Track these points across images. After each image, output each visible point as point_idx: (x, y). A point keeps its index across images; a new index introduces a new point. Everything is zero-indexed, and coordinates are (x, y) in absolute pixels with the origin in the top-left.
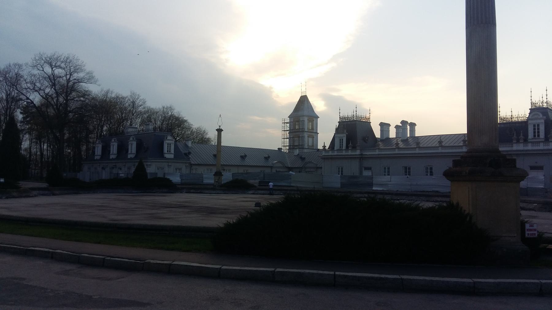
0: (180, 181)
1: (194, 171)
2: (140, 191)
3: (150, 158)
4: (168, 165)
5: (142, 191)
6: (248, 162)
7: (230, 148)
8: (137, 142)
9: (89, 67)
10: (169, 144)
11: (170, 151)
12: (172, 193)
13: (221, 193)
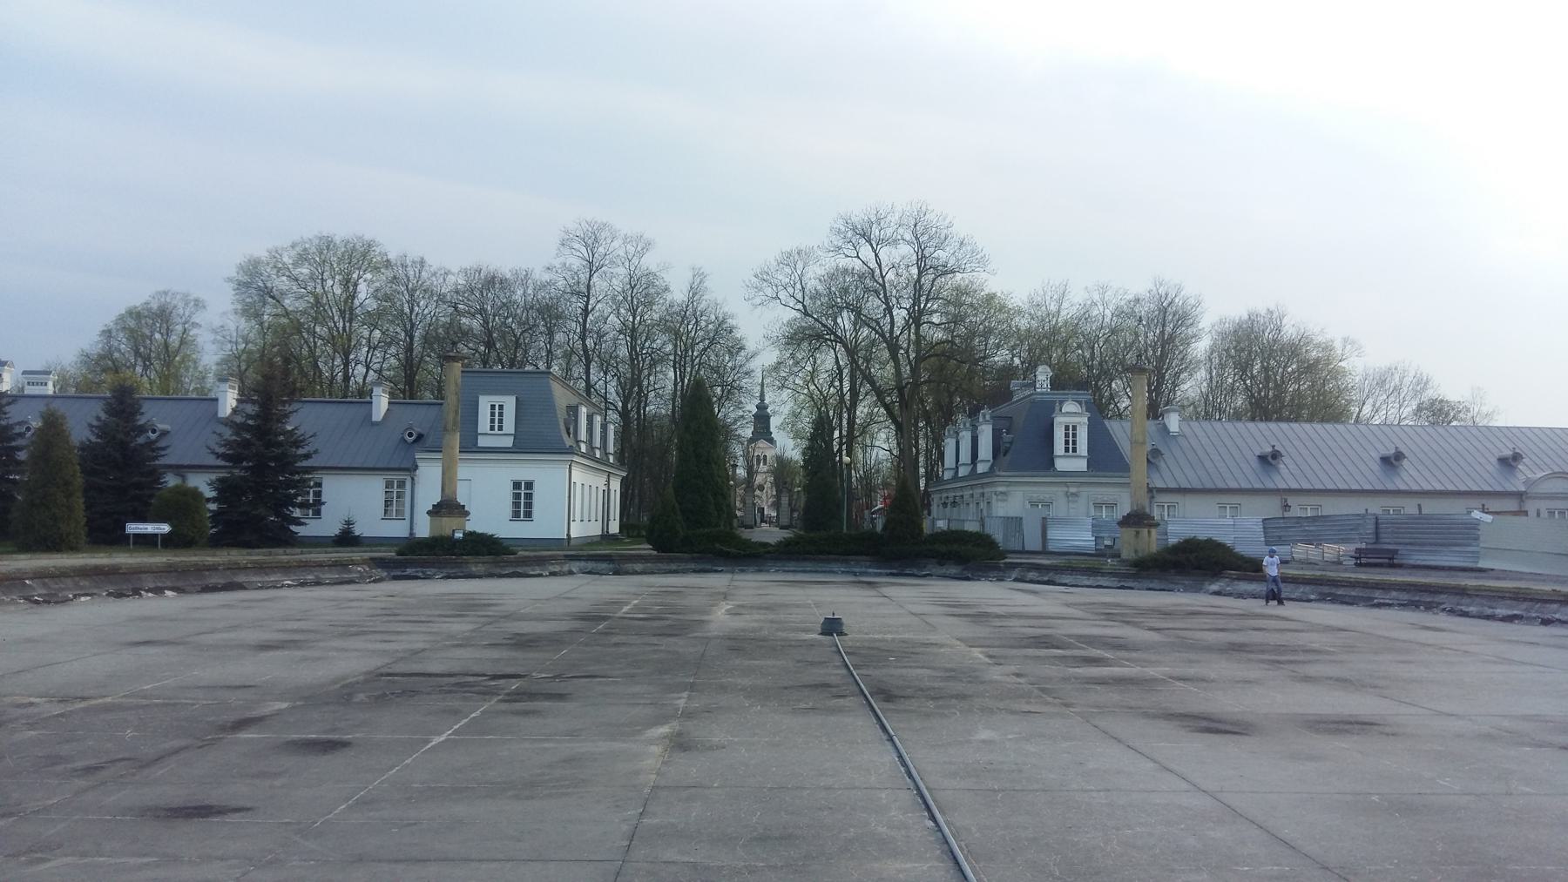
2: (889, 571)
3: (1004, 473)
4: (1067, 492)
5: (895, 571)
6: (1408, 475)
9: (960, 230)
11: (1074, 450)
12: (967, 579)
13: (1110, 585)
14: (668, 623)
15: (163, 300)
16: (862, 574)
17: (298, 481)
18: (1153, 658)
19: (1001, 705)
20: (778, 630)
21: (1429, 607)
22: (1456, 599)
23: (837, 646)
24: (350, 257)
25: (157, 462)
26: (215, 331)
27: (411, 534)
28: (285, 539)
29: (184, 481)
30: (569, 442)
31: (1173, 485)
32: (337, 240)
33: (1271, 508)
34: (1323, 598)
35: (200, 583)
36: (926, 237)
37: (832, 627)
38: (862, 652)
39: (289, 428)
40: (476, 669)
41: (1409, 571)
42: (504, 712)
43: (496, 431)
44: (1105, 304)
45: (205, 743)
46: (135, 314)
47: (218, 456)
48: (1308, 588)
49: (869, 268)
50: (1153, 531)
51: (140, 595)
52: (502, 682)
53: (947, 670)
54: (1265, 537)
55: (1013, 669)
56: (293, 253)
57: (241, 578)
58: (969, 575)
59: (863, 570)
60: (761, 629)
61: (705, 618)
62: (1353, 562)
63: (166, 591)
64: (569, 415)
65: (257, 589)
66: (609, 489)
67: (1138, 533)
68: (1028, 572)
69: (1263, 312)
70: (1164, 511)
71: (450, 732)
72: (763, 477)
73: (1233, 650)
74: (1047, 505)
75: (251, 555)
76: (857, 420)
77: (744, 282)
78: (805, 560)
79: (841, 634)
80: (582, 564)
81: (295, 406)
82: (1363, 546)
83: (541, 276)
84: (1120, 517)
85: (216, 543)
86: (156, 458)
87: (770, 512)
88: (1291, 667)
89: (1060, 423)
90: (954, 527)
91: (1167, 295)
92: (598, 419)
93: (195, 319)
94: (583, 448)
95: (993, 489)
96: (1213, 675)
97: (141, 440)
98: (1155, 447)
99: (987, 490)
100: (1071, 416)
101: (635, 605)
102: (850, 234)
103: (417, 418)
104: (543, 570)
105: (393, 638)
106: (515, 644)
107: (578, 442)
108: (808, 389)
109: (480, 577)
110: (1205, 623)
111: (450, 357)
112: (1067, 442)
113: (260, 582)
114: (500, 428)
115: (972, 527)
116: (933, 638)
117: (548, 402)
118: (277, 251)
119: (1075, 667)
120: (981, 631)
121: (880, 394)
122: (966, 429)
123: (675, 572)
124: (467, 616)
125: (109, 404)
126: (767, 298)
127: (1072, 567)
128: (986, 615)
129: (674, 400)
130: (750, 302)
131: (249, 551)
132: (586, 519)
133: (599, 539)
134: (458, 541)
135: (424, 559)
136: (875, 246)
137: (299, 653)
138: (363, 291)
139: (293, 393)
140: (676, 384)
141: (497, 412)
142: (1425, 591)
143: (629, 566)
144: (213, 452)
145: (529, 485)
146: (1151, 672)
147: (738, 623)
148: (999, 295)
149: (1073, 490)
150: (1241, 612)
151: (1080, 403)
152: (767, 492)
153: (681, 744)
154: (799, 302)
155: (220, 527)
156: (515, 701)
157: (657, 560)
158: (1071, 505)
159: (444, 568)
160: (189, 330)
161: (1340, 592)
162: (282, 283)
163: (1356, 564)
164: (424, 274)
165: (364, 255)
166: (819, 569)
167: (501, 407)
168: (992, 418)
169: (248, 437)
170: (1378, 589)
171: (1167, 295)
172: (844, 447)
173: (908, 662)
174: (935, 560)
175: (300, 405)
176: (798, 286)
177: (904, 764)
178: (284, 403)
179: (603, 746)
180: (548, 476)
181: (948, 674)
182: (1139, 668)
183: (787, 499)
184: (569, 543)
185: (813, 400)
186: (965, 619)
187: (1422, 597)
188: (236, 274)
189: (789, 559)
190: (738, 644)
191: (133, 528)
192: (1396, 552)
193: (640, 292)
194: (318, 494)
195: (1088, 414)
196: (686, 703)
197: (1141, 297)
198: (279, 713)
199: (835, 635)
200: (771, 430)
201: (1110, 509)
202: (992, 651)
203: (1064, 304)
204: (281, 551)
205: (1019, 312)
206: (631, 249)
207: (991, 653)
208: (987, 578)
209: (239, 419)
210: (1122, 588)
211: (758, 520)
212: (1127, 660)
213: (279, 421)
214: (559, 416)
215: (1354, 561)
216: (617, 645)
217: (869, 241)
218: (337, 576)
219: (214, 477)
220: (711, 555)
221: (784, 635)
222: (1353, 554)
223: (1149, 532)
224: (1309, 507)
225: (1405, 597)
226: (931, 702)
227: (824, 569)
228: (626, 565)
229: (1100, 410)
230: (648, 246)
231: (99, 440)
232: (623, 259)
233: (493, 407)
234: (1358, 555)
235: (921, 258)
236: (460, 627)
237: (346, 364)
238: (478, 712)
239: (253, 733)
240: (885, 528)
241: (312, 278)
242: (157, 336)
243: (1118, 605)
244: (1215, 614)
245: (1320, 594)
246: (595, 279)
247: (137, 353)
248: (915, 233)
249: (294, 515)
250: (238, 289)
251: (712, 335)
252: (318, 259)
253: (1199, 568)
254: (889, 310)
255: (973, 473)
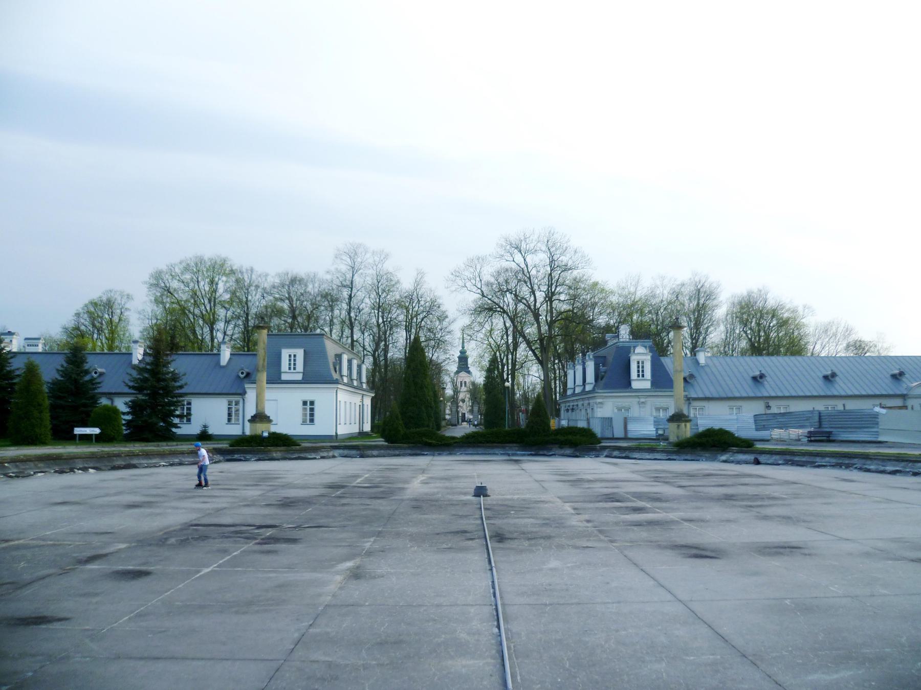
0: (655, 432)
1: (661, 414)
2: (530, 453)
3: (601, 391)
4: (639, 402)
5: (533, 453)
6: (841, 386)
7: (850, 361)
8: (595, 361)
9: (574, 243)
10: (292, 356)
11: (643, 376)
14: (381, 489)
15: (109, 295)
16: (513, 455)
17: (176, 402)
18: (675, 506)
19: (571, 543)
20: (448, 494)
21: (848, 466)
22: (863, 461)
23: (481, 505)
24: (214, 267)
25: (96, 391)
26: (139, 313)
27: (243, 433)
28: (167, 435)
29: (112, 403)
30: (336, 376)
31: (701, 396)
32: (206, 258)
33: (758, 408)
34: (786, 463)
35: (110, 464)
36: (554, 249)
37: (480, 491)
38: (495, 508)
39: (172, 370)
40: (251, 521)
41: (839, 444)
42: (255, 552)
43: (292, 370)
44: (664, 287)
45: (65, 571)
46: (95, 304)
47: (130, 387)
48: (777, 457)
49: (520, 267)
50: (688, 425)
51: (74, 472)
52: (263, 530)
53: (545, 519)
54: (756, 426)
55: (587, 517)
56: (181, 267)
57: (135, 461)
58: (578, 454)
59: (513, 452)
60: (438, 493)
61: (406, 486)
62: (806, 439)
63: (90, 469)
64: (336, 360)
65: (144, 468)
66: (363, 405)
67: (678, 426)
68: (614, 451)
69: (756, 291)
70: (696, 411)
71: (215, 565)
72: (463, 394)
73: (726, 499)
74: (628, 409)
75: (147, 446)
76: (517, 359)
77: (445, 277)
78: (479, 447)
79: (486, 495)
80: (341, 451)
81: (174, 357)
82: (812, 429)
83: (323, 275)
84: (668, 417)
85: (129, 439)
86: (95, 389)
87: (469, 416)
88: (758, 510)
89: (634, 359)
90: (572, 424)
91: (700, 281)
92: (355, 363)
93: (127, 306)
94: (345, 380)
95: (594, 401)
96: (708, 517)
97: (87, 378)
98: (691, 373)
99: (591, 401)
100: (641, 356)
101: (366, 478)
102: (508, 247)
103: (245, 363)
104: (316, 455)
105: (209, 500)
106: (282, 505)
107: (342, 376)
108: (488, 340)
109: (278, 460)
110: (713, 481)
111: (260, 326)
112: (638, 371)
113: (146, 463)
114: (295, 369)
115: (582, 424)
116: (543, 497)
117: (323, 353)
118: (172, 266)
119: (625, 514)
120: (575, 492)
121: (529, 343)
122: (579, 364)
123: (398, 455)
124: (260, 485)
125: (68, 357)
126: (459, 287)
127: (639, 448)
128: (580, 481)
129: (406, 349)
130: (449, 289)
131: (146, 444)
132: (348, 422)
133: (356, 435)
134: (265, 438)
135: (244, 449)
136: (523, 254)
137: (148, 511)
138: (221, 287)
139: (174, 347)
140: (407, 339)
141: (293, 359)
142: (845, 457)
143: (369, 452)
144: (127, 385)
145: (312, 403)
146: (672, 516)
147: (425, 489)
148: (600, 282)
149: (642, 400)
150: (735, 473)
151: (645, 347)
152: (466, 403)
153: (356, 575)
154: (479, 288)
155: (132, 429)
156: (265, 544)
157: (387, 448)
158: (641, 409)
159: (257, 454)
160: (124, 312)
161: (797, 459)
162: (175, 284)
163: (808, 440)
164: (254, 277)
165: (222, 266)
166: (487, 452)
167: (295, 356)
168: (595, 357)
169: (147, 376)
170: (819, 456)
171: (700, 281)
172: (510, 376)
173: (522, 514)
174: (557, 446)
175: (176, 356)
176: (478, 279)
177: (494, 587)
178: (167, 355)
179: (308, 576)
180: (321, 395)
181: (544, 522)
182: (665, 514)
183: (477, 408)
184: (337, 437)
185: (491, 348)
186: (567, 484)
187: (844, 461)
188: (149, 280)
189: (469, 447)
190: (419, 504)
191: (78, 431)
192: (830, 433)
193: (384, 284)
194: (189, 409)
195: (651, 354)
196: (371, 545)
197: (685, 283)
198: (119, 551)
199: (482, 496)
200: (469, 366)
201: (665, 411)
202: (576, 505)
203: (638, 287)
204: (164, 444)
205: (612, 292)
206: (377, 259)
207: (576, 506)
208: (589, 456)
209: (142, 366)
210: (669, 459)
211: (460, 421)
212: (658, 508)
213: (164, 366)
214: (330, 361)
215: (806, 439)
216: (344, 505)
217: (520, 251)
218: (193, 460)
219: (128, 399)
220: (420, 445)
221: (450, 497)
222: (806, 434)
223: (685, 425)
224: (782, 407)
225: (834, 461)
226: (527, 542)
227: (490, 452)
228: (368, 452)
229: (660, 350)
230: (387, 256)
231: (62, 379)
232: (372, 265)
233: (290, 356)
234: (809, 435)
235: (552, 261)
236: (254, 493)
237: (212, 330)
238: (239, 552)
239: (95, 565)
240: (527, 426)
241: (192, 279)
242: (107, 316)
243: (664, 471)
244: (717, 475)
245: (785, 460)
246: (356, 277)
247: (94, 326)
248: (547, 245)
249: (174, 422)
250: (150, 288)
251: (428, 309)
252: (195, 270)
253: (714, 446)
254: (533, 292)
255: (584, 392)
